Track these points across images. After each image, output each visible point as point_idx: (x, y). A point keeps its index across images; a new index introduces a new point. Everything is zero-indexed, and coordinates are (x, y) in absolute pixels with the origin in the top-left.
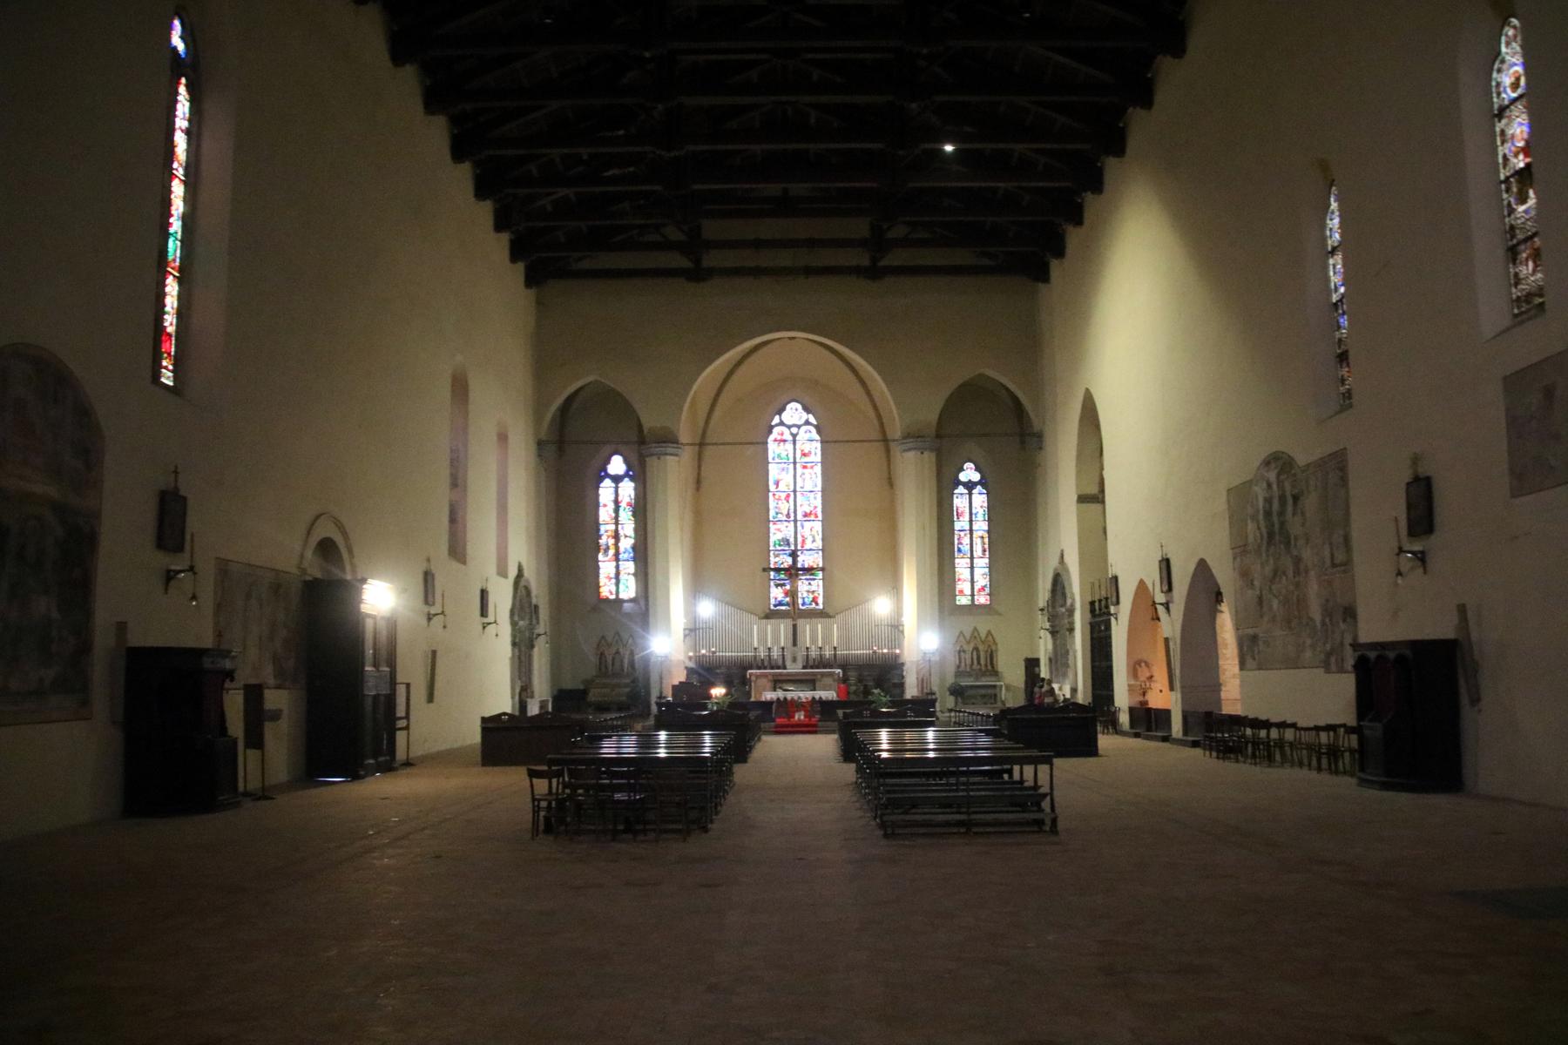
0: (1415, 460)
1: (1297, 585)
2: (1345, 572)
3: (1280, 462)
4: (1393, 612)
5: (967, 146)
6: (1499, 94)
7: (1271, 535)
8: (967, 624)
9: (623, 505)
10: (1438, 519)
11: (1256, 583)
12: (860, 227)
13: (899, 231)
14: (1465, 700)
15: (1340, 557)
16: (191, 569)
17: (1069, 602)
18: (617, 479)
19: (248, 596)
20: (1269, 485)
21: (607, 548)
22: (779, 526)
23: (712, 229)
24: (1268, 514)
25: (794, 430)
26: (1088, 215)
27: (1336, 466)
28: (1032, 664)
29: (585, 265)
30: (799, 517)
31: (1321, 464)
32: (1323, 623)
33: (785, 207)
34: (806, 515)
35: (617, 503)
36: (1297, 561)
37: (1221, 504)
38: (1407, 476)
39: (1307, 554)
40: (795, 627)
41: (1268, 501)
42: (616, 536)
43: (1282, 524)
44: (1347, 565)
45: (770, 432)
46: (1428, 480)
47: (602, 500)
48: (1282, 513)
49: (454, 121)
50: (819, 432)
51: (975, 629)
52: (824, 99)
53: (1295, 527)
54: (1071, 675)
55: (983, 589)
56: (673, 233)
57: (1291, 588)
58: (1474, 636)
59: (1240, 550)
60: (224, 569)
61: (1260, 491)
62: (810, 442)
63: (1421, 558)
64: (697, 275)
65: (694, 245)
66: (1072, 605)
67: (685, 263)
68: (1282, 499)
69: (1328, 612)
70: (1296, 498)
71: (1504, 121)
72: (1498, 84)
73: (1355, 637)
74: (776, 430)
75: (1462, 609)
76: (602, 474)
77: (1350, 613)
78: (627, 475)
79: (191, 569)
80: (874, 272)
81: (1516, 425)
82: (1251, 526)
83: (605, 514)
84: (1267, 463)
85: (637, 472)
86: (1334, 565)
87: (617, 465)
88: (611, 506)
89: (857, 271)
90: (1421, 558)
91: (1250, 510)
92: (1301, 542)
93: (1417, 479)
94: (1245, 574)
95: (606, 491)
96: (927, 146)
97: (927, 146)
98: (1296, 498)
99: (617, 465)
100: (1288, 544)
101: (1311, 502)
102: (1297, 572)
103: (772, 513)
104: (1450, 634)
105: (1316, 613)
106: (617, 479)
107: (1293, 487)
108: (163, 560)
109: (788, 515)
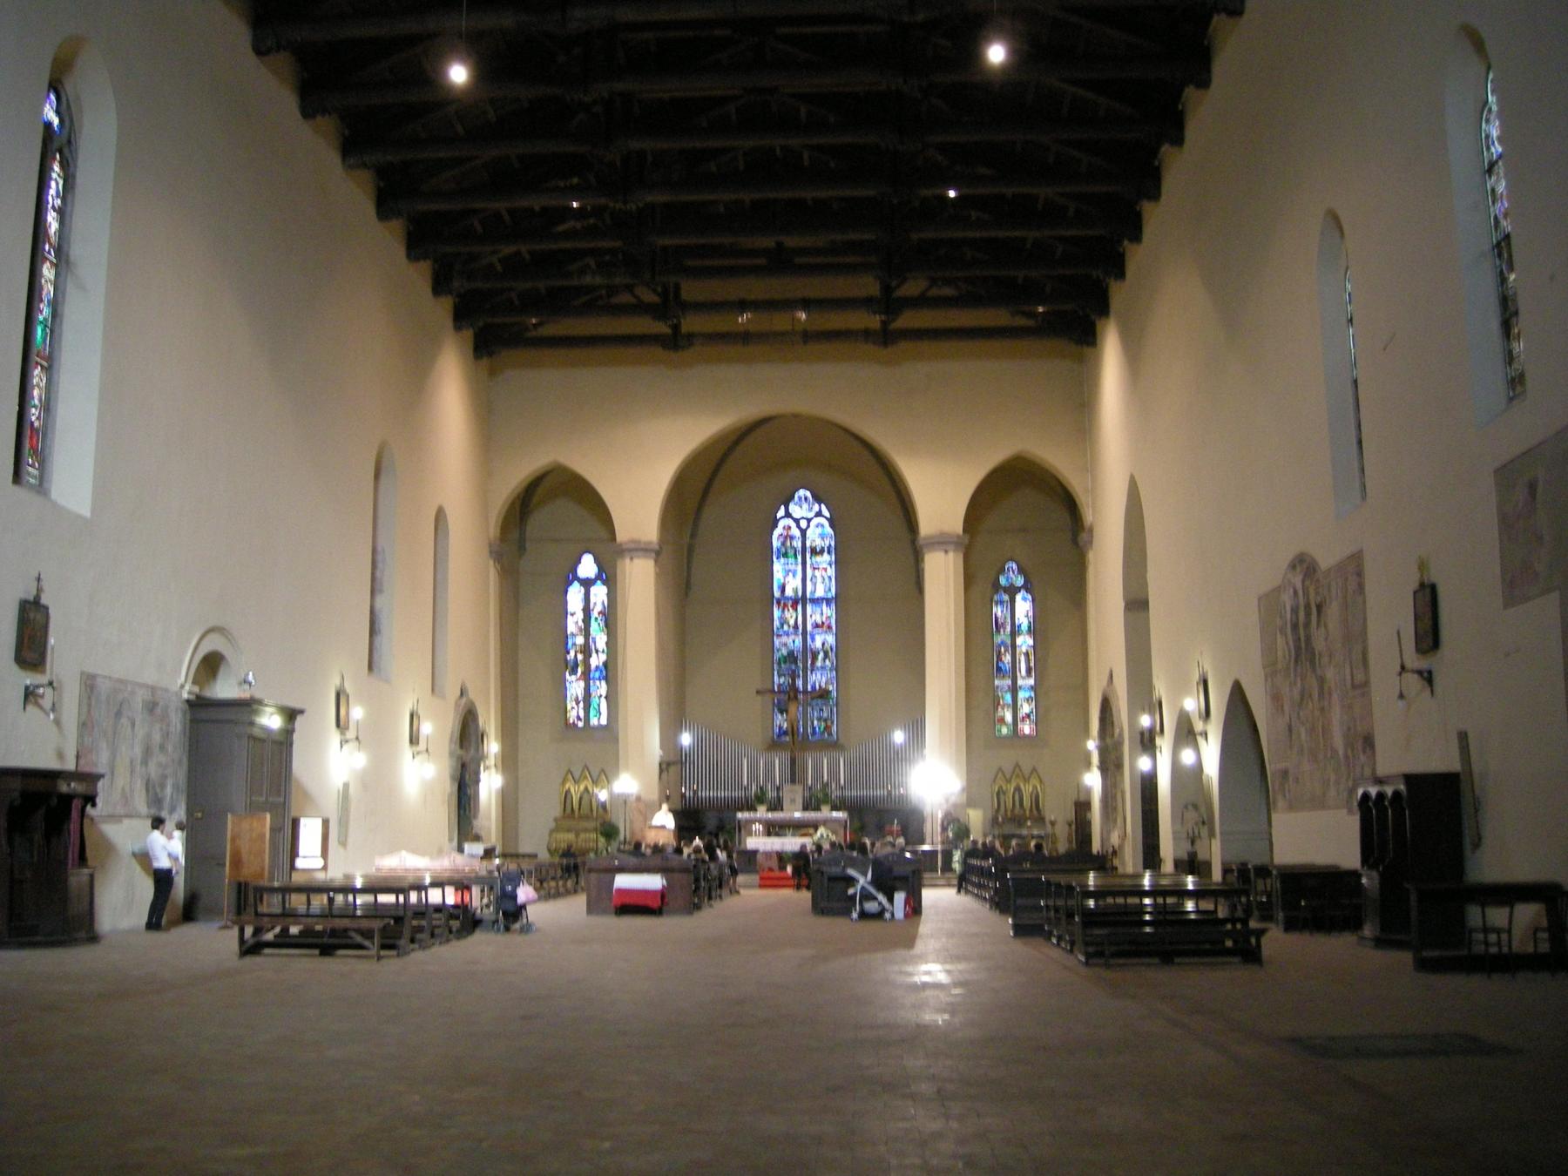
0: (1422, 566)
1: (1322, 709)
2: (1363, 695)
3: (1304, 565)
4: (1408, 746)
5: (970, 191)
6: (1488, 148)
7: (1298, 649)
8: (1006, 758)
9: (595, 614)
10: (1445, 634)
11: (1286, 708)
12: (868, 285)
13: (913, 287)
14: (1467, 842)
15: (1360, 677)
16: (51, 684)
17: (1117, 731)
18: (587, 584)
19: (118, 714)
20: (1295, 592)
21: (576, 665)
22: (784, 639)
23: (692, 290)
24: (1295, 627)
25: (803, 524)
26: (1131, 268)
27: (1354, 566)
28: (1083, 806)
29: (549, 330)
30: (809, 628)
31: (1340, 567)
32: (1346, 757)
33: (780, 262)
34: (817, 626)
35: (587, 611)
36: (1322, 680)
37: (1253, 617)
38: (1413, 584)
39: (1330, 674)
40: (793, 761)
41: (1295, 611)
42: (586, 650)
43: (1308, 639)
44: (1366, 684)
45: (775, 526)
46: (1433, 588)
47: (570, 609)
48: (1307, 625)
49: (382, 172)
50: (832, 526)
51: (1017, 765)
52: (815, 141)
53: (1319, 644)
54: (1120, 821)
55: (1028, 716)
56: (649, 297)
57: (1317, 713)
58: (1476, 768)
59: (1271, 671)
60: (89, 683)
61: (1287, 598)
62: (820, 532)
63: (1428, 677)
64: (675, 341)
65: (669, 305)
66: (1121, 735)
67: (662, 328)
68: (1307, 606)
69: (1349, 744)
70: (1319, 607)
71: (1494, 178)
72: (1487, 137)
73: (1374, 770)
74: (782, 523)
75: (1463, 737)
76: (571, 576)
77: (1369, 742)
78: (599, 577)
79: (51, 684)
80: (886, 337)
81: (1506, 524)
82: (1280, 640)
83: (573, 624)
84: (1293, 566)
85: (607, 575)
86: (1354, 687)
87: (587, 567)
88: (580, 615)
89: (867, 334)
90: (1428, 677)
91: (1279, 622)
92: (1325, 660)
93: (1422, 585)
94: (1276, 698)
95: (575, 595)
96: (926, 192)
97: (926, 192)
98: (1319, 607)
99: (587, 567)
100: (1312, 663)
101: (1333, 611)
102: (1321, 694)
103: (776, 623)
104: (1454, 765)
105: (1338, 742)
106: (587, 584)
107: (1317, 593)
108: (29, 679)
109: (796, 626)
